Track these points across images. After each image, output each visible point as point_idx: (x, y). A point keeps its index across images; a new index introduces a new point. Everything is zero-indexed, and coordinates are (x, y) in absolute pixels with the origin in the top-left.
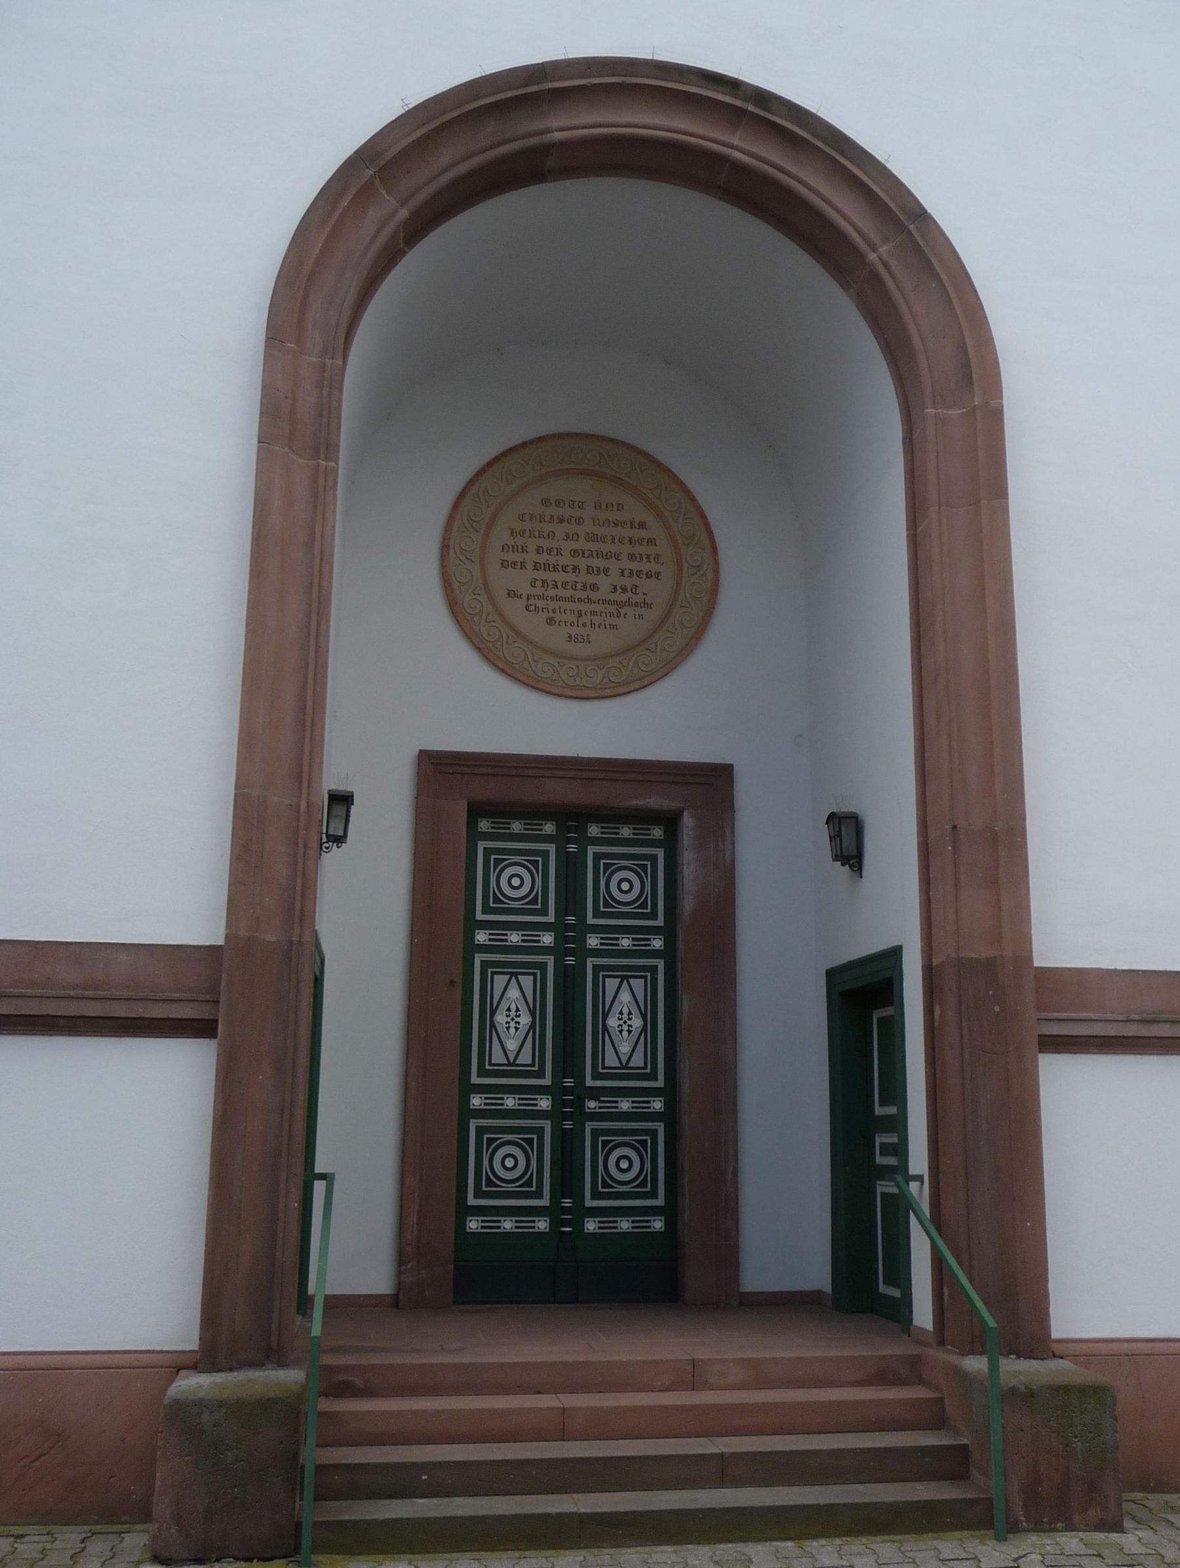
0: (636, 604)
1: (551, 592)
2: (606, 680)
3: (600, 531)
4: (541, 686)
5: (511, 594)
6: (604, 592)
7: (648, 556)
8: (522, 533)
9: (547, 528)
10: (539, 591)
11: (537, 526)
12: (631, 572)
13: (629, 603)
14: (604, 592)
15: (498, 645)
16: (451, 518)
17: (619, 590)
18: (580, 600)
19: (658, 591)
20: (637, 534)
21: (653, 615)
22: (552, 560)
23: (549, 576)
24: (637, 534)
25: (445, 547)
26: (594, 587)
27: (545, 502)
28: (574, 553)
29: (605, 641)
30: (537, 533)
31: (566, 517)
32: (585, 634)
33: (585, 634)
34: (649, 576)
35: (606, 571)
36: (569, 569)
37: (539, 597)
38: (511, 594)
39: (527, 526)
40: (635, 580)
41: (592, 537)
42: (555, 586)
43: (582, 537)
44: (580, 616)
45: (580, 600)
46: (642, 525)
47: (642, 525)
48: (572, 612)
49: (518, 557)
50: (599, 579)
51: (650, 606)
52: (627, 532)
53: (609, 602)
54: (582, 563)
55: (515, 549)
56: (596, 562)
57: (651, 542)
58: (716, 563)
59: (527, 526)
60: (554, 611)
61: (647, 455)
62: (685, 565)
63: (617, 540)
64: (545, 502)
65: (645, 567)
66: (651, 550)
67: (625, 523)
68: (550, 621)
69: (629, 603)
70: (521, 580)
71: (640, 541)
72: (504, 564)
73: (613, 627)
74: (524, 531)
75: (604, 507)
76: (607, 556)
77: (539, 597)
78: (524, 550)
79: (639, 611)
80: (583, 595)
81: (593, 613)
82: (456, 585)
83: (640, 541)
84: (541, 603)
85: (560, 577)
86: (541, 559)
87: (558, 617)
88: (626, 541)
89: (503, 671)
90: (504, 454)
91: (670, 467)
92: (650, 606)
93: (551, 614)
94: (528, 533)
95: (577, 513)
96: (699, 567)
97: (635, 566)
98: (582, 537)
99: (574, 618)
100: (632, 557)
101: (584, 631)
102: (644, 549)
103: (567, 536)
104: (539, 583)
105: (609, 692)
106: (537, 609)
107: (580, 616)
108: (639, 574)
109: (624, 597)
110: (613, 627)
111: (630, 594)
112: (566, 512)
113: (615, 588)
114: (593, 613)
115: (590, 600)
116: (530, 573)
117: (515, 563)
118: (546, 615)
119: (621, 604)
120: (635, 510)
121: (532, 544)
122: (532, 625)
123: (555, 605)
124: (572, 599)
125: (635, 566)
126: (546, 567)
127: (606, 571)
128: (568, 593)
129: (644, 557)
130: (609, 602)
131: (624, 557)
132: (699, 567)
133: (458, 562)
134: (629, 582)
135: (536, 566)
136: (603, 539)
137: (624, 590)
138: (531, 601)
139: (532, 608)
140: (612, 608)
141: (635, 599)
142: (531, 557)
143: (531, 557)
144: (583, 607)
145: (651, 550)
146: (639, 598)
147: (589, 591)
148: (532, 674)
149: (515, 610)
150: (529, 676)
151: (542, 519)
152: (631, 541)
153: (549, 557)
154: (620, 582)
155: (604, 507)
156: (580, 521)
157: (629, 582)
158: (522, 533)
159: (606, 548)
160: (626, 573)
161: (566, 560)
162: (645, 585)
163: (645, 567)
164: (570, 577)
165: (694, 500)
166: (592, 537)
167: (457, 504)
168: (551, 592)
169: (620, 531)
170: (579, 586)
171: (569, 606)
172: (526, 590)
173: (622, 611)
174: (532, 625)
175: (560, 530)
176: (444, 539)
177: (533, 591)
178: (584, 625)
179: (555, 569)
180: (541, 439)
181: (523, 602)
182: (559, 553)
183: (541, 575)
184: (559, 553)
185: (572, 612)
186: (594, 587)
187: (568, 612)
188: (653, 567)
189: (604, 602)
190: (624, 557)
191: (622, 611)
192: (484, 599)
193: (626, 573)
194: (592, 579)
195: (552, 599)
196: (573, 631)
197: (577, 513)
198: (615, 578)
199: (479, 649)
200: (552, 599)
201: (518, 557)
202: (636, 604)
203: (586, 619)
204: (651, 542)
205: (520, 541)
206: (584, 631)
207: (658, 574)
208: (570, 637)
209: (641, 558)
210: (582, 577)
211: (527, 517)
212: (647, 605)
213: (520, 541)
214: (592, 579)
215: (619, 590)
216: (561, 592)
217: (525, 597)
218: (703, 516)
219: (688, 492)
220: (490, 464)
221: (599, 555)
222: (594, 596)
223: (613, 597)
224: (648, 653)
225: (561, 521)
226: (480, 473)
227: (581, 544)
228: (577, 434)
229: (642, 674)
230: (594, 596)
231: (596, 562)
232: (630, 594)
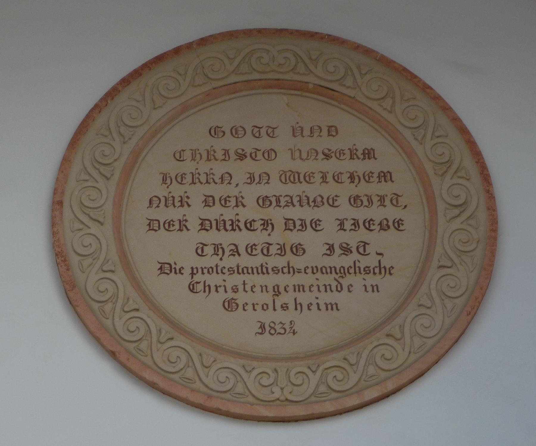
0: (367, 270)
1: (230, 262)
2: (323, 388)
3: (303, 167)
4: (215, 404)
5: (166, 268)
6: (315, 254)
7: (382, 199)
8: (180, 179)
9: (219, 168)
10: (210, 261)
11: (204, 167)
12: (356, 224)
13: (355, 269)
14: (315, 254)
15: (144, 345)
16: (66, 162)
17: (338, 251)
18: (276, 270)
19: (401, 249)
20: (361, 167)
21: (394, 285)
22: (229, 214)
23: (225, 238)
24: (361, 167)
25: (57, 204)
26: (298, 250)
27: (215, 132)
28: (264, 201)
29: (316, 330)
30: (203, 178)
31: (248, 151)
32: (287, 321)
33: (287, 321)
34: (384, 227)
35: (315, 225)
36: (257, 225)
37: (210, 271)
38: (166, 268)
39: (188, 167)
40: (362, 234)
41: (290, 177)
42: (236, 252)
43: (275, 178)
44: (277, 292)
45: (276, 270)
46: (369, 154)
47: (369, 154)
48: (264, 288)
49: (174, 214)
50: (307, 238)
51: (390, 271)
52: (347, 165)
53: (323, 270)
54: (277, 215)
55: (169, 202)
56: (296, 213)
57: (385, 176)
58: (490, 196)
59: (188, 167)
60: (235, 290)
61: (368, 52)
62: (441, 206)
63: (330, 178)
64: (215, 132)
65: (377, 213)
66: (386, 189)
67: (342, 152)
68: (230, 305)
69: (355, 269)
70: (180, 248)
71: (368, 177)
72: (152, 225)
73: (333, 307)
74: (183, 176)
75: (307, 132)
76: (316, 203)
77: (210, 271)
78: (184, 202)
79: (371, 280)
80: (280, 262)
81: (299, 288)
82: (74, 259)
83: (368, 177)
84: (213, 280)
85: (243, 238)
86: (214, 213)
87: (241, 298)
88: (345, 178)
89: (153, 386)
90: (148, 66)
91: (317, 31)
92: (390, 271)
93: (230, 295)
94: (189, 178)
95: (265, 143)
96: (464, 205)
97: (362, 214)
98: (275, 178)
99: (267, 298)
100: (355, 201)
101: (280, 316)
102: (374, 189)
103: (251, 179)
104: (209, 250)
105: (329, 407)
106: (207, 288)
107: (277, 292)
108: (368, 224)
109: (347, 261)
110: (333, 307)
111: (355, 256)
112: (248, 143)
113: (331, 248)
114: (299, 288)
115: (291, 269)
116: (195, 236)
117: (170, 223)
118: (222, 296)
119: (344, 272)
120: (356, 132)
121: (197, 194)
122: (201, 313)
123: (237, 279)
124: (263, 270)
125: (362, 214)
126: (220, 225)
127: (315, 225)
128: (257, 261)
129: (375, 199)
130: (323, 270)
131: (343, 201)
132: (464, 205)
133: (78, 226)
134: (352, 239)
135: (204, 225)
136: (308, 178)
137: (346, 250)
138: (198, 277)
139: (200, 287)
140: (329, 279)
141: (364, 262)
142: (195, 212)
143: (195, 212)
144: (283, 280)
145: (386, 189)
146: (371, 261)
147: (289, 256)
148: (198, 385)
149: (170, 292)
150: (193, 390)
151: (210, 156)
152: (352, 177)
153: (223, 210)
154: (339, 238)
155: (307, 132)
156: (270, 154)
157: (352, 239)
158: (180, 179)
159: (313, 190)
160: (348, 225)
161: (251, 212)
162: (377, 239)
163: (377, 213)
164: (259, 237)
165: (446, 109)
166: (290, 177)
167: (74, 142)
168: (230, 262)
169: (331, 166)
170: (273, 249)
171: (259, 280)
172: (188, 259)
173: (345, 282)
174: (201, 313)
175: (239, 170)
176: (55, 191)
177: (199, 262)
178: (285, 307)
179: (235, 226)
180: (203, 42)
181: (186, 279)
182: (239, 203)
183: (212, 237)
184: (239, 203)
185: (264, 288)
186: (298, 250)
187: (257, 289)
188: (391, 213)
189: (315, 270)
190: (343, 201)
191: (345, 282)
192: (120, 277)
193: (348, 225)
194: (294, 237)
195: (231, 271)
196: (267, 317)
197: (265, 143)
198: (331, 234)
199: (113, 355)
200: (231, 271)
201: (174, 214)
202: (367, 270)
203: (287, 298)
204: (385, 176)
205: (177, 190)
206: (280, 316)
207: (398, 224)
208: (262, 327)
209: (370, 201)
210: (278, 236)
211: (187, 155)
212: (382, 270)
213: (177, 190)
214: (294, 237)
215: (338, 251)
216: (245, 260)
217: (187, 271)
218: (464, 131)
219: (437, 99)
220: (126, 82)
221: (304, 201)
222: (298, 262)
223: (328, 262)
224: (390, 341)
225: (242, 157)
226: (112, 94)
227: (275, 188)
228: (260, 31)
229: (383, 375)
230: (298, 262)
231: (296, 213)
232: (355, 256)
